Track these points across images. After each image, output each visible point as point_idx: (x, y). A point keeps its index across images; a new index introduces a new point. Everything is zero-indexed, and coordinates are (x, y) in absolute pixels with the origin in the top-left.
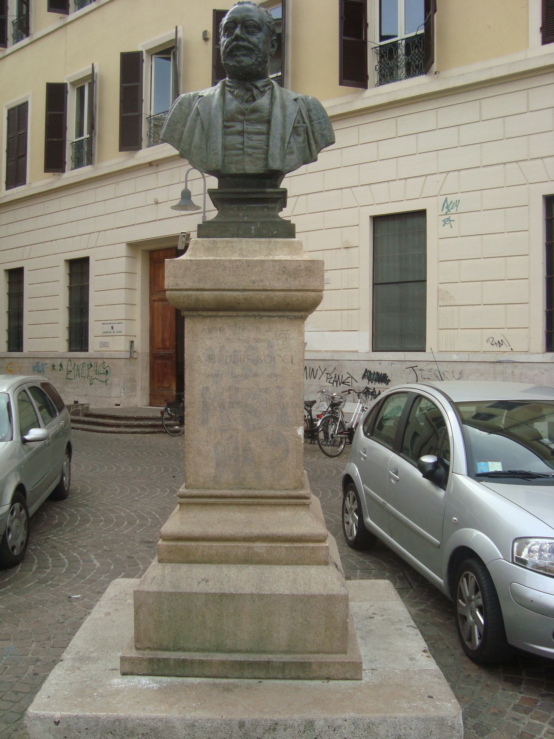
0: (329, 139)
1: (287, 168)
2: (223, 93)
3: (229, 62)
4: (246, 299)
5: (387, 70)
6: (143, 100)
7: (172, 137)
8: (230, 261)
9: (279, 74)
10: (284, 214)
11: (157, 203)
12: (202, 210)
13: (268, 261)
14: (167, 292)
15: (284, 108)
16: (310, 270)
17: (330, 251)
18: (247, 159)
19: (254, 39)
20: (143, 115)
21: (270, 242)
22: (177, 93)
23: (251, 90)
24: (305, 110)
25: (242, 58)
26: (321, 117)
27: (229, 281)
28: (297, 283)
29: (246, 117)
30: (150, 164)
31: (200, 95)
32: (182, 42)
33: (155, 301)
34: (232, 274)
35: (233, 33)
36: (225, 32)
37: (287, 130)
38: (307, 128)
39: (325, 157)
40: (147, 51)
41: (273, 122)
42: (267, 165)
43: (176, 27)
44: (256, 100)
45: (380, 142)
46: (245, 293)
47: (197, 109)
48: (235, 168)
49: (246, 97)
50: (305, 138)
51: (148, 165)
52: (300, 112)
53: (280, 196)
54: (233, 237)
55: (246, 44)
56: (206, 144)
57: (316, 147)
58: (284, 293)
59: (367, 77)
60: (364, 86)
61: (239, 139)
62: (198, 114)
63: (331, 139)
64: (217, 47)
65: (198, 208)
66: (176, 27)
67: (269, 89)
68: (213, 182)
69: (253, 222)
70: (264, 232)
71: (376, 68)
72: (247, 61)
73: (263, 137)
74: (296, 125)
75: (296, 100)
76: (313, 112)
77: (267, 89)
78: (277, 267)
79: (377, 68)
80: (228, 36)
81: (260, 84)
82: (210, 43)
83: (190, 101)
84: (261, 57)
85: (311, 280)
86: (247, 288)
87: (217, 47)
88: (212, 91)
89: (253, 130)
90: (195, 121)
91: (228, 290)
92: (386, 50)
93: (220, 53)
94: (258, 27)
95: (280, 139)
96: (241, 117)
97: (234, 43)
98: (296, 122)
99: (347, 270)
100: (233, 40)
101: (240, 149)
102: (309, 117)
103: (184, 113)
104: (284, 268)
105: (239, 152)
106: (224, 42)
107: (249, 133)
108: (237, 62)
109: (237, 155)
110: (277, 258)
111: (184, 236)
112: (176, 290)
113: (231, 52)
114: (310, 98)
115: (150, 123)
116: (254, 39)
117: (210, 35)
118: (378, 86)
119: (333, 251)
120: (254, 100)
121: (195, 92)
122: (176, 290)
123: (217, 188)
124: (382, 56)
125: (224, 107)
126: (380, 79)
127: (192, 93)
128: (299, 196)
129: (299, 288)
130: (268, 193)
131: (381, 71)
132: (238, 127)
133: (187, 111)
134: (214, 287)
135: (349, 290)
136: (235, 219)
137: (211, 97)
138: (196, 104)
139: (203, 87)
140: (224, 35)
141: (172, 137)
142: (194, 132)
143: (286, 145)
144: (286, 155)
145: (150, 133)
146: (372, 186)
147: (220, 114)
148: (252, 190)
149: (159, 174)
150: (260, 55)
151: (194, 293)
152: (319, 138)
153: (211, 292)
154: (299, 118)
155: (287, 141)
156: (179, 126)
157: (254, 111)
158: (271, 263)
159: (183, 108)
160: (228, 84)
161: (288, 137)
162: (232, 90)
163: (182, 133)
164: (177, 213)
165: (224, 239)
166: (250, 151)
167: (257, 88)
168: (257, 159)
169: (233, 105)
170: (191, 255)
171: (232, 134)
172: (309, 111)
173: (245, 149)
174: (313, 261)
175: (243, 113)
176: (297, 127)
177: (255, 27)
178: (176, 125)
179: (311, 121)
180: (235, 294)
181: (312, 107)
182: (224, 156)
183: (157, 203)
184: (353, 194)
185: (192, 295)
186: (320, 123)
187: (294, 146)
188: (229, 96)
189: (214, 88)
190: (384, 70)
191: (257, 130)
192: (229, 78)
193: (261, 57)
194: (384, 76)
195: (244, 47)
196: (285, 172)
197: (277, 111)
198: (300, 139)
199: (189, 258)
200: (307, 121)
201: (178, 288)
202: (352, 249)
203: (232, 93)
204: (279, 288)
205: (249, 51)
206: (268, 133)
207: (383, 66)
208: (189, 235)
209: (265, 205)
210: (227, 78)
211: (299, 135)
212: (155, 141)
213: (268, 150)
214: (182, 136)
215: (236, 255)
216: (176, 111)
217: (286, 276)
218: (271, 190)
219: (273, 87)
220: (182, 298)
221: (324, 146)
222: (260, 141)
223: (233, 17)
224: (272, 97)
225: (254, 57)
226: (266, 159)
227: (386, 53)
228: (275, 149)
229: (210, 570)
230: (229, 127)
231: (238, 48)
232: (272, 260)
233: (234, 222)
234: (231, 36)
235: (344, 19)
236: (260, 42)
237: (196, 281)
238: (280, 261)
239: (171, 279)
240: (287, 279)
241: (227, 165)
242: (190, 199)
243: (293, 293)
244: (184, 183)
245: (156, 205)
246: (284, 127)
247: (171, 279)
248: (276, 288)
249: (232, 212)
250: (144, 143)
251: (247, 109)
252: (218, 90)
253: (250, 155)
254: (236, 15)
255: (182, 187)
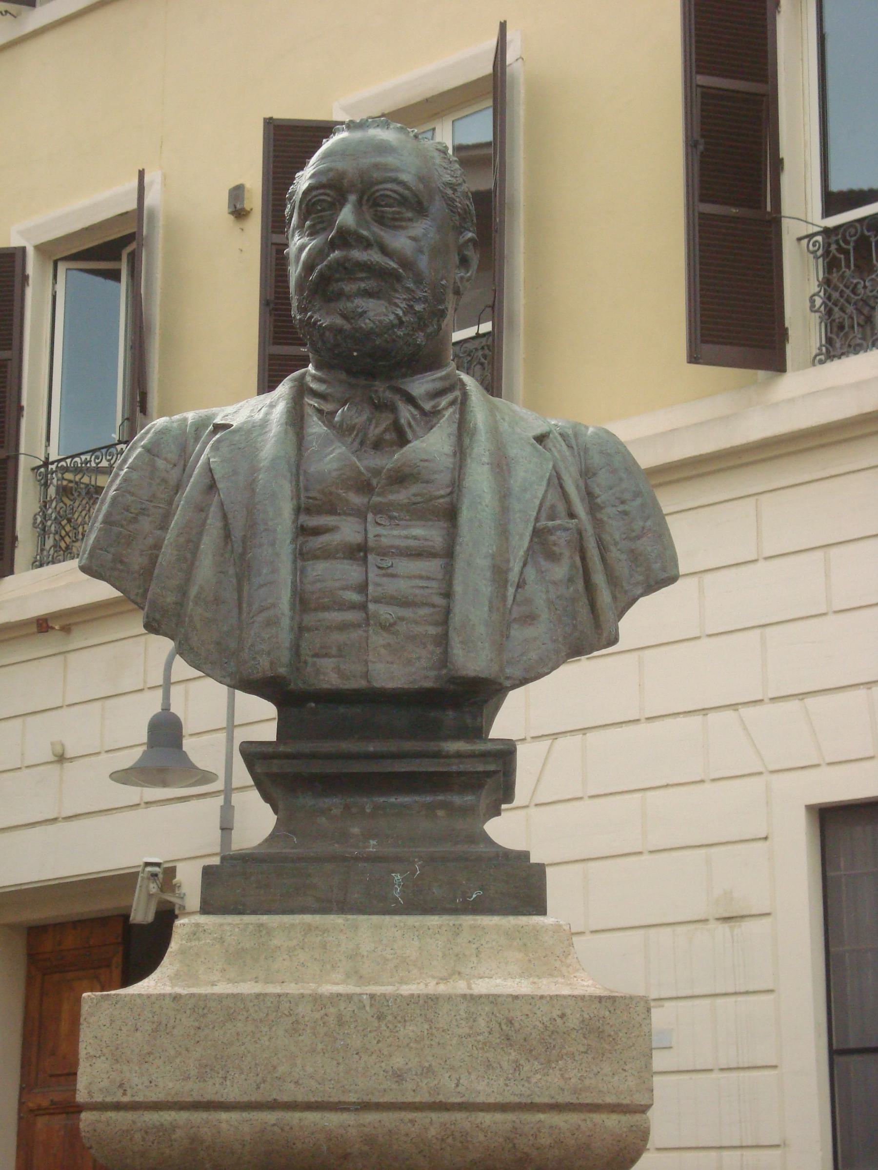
0: (657, 566)
1: (514, 671)
2: (296, 418)
3: (316, 316)
4: (370, 1140)
5: (850, 309)
6: (20, 409)
7: (121, 562)
8: (317, 999)
9: (486, 327)
10: (504, 830)
11: (61, 758)
12: (219, 785)
13: (450, 998)
14: (84, 1115)
15: (501, 466)
16: (600, 1034)
17: (668, 930)
18: (378, 639)
19: (400, 241)
20: (22, 458)
21: (457, 931)
22: (139, 403)
23: (393, 409)
24: (574, 470)
25: (362, 303)
26: (627, 496)
27: (310, 1072)
28: (554, 1079)
29: (376, 499)
30: (43, 625)
31: (218, 420)
32: (161, 222)
33: (39, 1111)
34: (320, 1046)
35: (331, 223)
36: (303, 219)
37: (514, 541)
38: (580, 533)
39: (644, 619)
40: (38, 248)
41: (465, 515)
42: (445, 660)
43: (141, 174)
44: (408, 442)
45: (834, 551)
46: (370, 1117)
47: (209, 470)
48: (338, 670)
49: (374, 432)
50: (573, 566)
51: (34, 629)
52: (556, 481)
53: (491, 768)
54: (324, 908)
55: (374, 256)
56: (240, 590)
57: (614, 598)
58: (510, 1117)
59: (783, 335)
60: (775, 362)
61: (351, 572)
62: (212, 487)
63: (664, 569)
64: (277, 238)
65: (206, 777)
66: (141, 174)
67: (452, 403)
68: (260, 719)
69: (398, 859)
70: (437, 892)
71: (812, 301)
72: (377, 312)
73: (433, 566)
74: (543, 523)
75: (541, 439)
76: (603, 478)
77: (444, 402)
78: (482, 1023)
79: (818, 301)
80: (313, 233)
81: (420, 386)
82: (255, 225)
83: (185, 442)
84: (425, 300)
85: (607, 1069)
86: (374, 1099)
87: (277, 238)
88: (259, 411)
89: (397, 542)
90: (202, 509)
91: (309, 1107)
92: (847, 242)
93: (287, 282)
94: (415, 204)
95: (488, 574)
96: (356, 499)
97: (336, 254)
98: (544, 515)
99: (732, 999)
100: (332, 245)
101: (353, 606)
102: (589, 496)
103: (164, 481)
104: (511, 1028)
105: (351, 616)
106: (302, 248)
107: (383, 552)
108: (344, 316)
109: (343, 627)
110: (481, 987)
111: (155, 875)
112: (118, 1107)
113: (324, 285)
114: (591, 430)
115: (46, 485)
116: (400, 241)
117: (255, 201)
118: (821, 362)
119: (680, 929)
120: (402, 440)
121: (203, 412)
122: (118, 1107)
123: (273, 737)
124: (831, 265)
125: (298, 466)
126: (829, 341)
127: (191, 416)
128: (555, 736)
129: (561, 1099)
130: (448, 756)
131: (829, 312)
132: (348, 531)
133: (174, 475)
134: (255, 1097)
135: (742, 1074)
136: (337, 848)
137: (253, 431)
138: (206, 454)
139: (226, 392)
140: (300, 226)
141: (121, 562)
142: (197, 547)
143: (511, 590)
144: (508, 627)
145: (45, 517)
146: (809, 701)
147: (287, 489)
148: (391, 746)
149: (71, 657)
150: (420, 294)
151: (183, 1116)
152: (622, 567)
153: (245, 1115)
154: (553, 497)
155: (514, 576)
156: (145, 524)
157: (401, 478)
158: (463, 1007)
159: (160, 463)
160: (314, 386)
161: (516, 567)
162: (327, 407)
163: (157, 546)
164: (133, 793)
165: (297, 919)
166: (386, 612)
167: (411, 400)
168: (412, 638)
169: (332, 457)
170: (176, 978)
171: (327, 554)
172: (587, 473)
173: (372, 607)
174: (613, 999)
175: (365, 487)
176: (550, 531)
177: (403, 202)
178: (135, 520)
179: (594, 507)
180: (333, 1120)
181: (596, 460)
182: (300, 630)
183: (61, 758)
184: (745, 729)
185: (174, 1127)
186: (625, 513)
187: (538, 595)
188: (316, 427)
189: (268, 398)
190: (842, 309)
191: (412, 543)
192: (317, 368)
193: (425, 300)
194: (841, 327)
195: (368, 268)
196: (508, 683)
197: (480, 479)
198: (560, 571)
199: (168, 990)
200: (580, 509)
201: (126, 1099)
202: (747, 926)
203: (326, 416)
204: (491, 1100)
205: (385, 280)
206: (449, 553)
207: (836, 295)
208: (171, 872)
209: (440, 798)
210: (311, 368)
211: (552, 557)
212: (56, 548)
213: (448, 611)
214: (153, 561)
215: (338, 976)
216: (135, 476)
217: (514, 1055)
218: (460, 746)
219: (465, 395)
220: (138, 1136)
221: (639, 591)
222: (421, 577)
223: (330, 170)
224: (463, 430)
225: (401, 299)
226: (443, 640)
227: (846, 253)
228: (474, 607)
229: (286, 347)
230: (317, 532)
231: (346, 269)
232: (464, 996)
233: (333, 858)
234: (324, 229)
235: (701, 148)
236: (420, 251)
237: (194, 1072)
238: (493, 999)
239: (101, 1065)
240: (518, 1067)
241: (310, 660)
242: (180, 746)
243: (541, 1116)
244: (160, 693)
245: (56, 767)
246: (504, 532)
247: (101, 1065)
248: (481, 1099)
249: (322, 821)
250: (24, 550)
251: (377, 472)
252: (281, 408)
253: (387, 627)
254: (340, 166)
255: (152, 705)
